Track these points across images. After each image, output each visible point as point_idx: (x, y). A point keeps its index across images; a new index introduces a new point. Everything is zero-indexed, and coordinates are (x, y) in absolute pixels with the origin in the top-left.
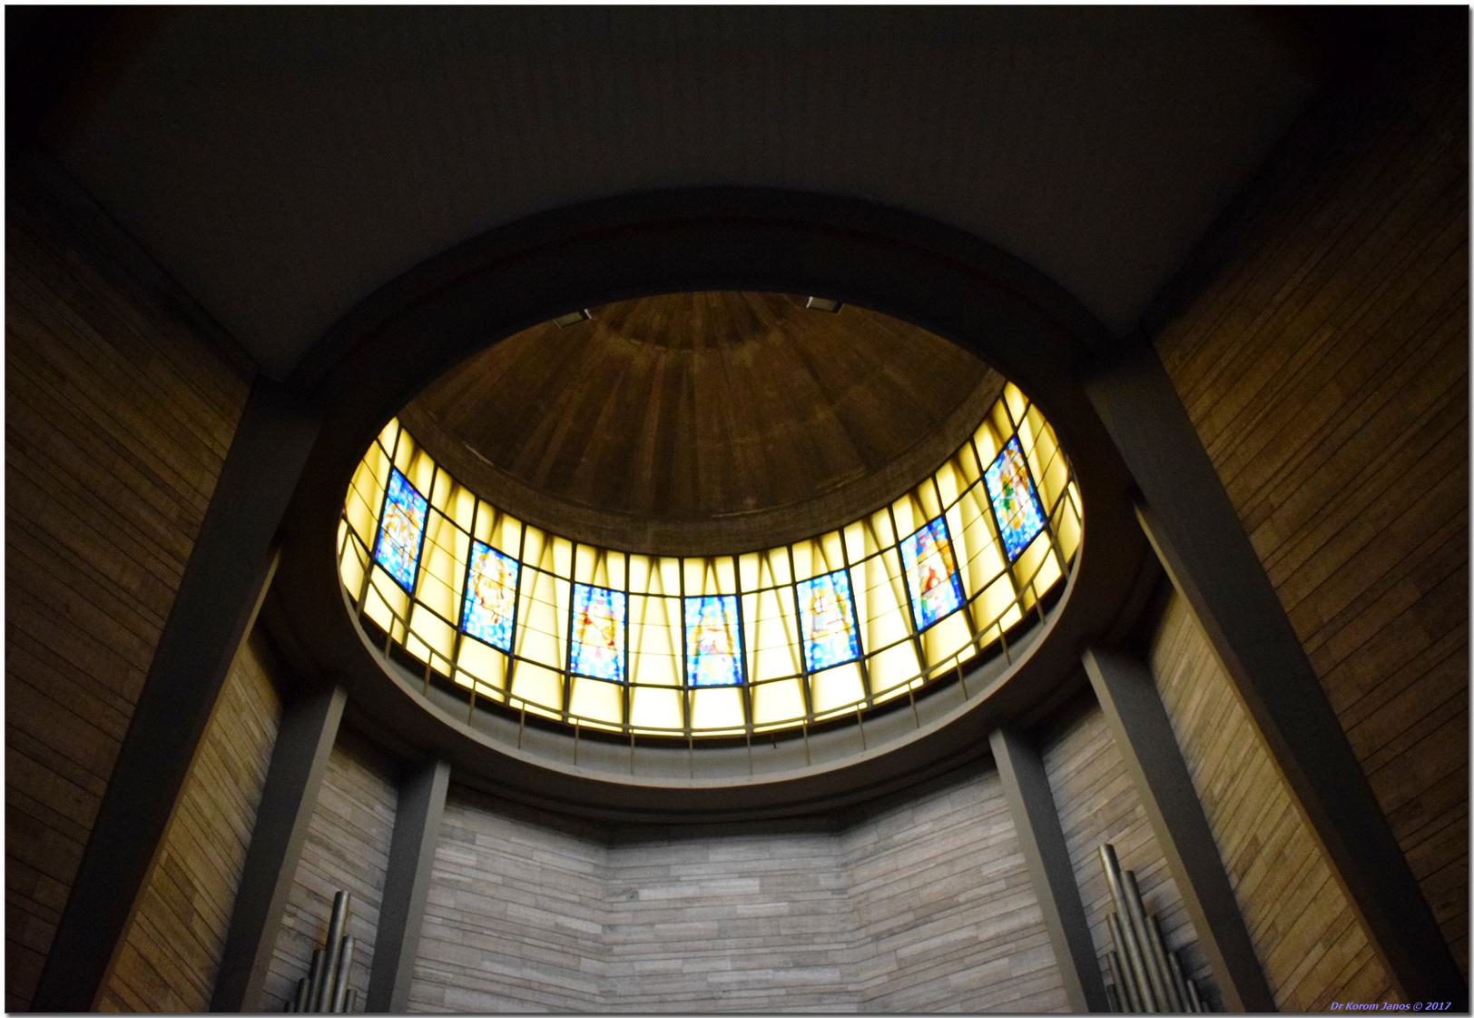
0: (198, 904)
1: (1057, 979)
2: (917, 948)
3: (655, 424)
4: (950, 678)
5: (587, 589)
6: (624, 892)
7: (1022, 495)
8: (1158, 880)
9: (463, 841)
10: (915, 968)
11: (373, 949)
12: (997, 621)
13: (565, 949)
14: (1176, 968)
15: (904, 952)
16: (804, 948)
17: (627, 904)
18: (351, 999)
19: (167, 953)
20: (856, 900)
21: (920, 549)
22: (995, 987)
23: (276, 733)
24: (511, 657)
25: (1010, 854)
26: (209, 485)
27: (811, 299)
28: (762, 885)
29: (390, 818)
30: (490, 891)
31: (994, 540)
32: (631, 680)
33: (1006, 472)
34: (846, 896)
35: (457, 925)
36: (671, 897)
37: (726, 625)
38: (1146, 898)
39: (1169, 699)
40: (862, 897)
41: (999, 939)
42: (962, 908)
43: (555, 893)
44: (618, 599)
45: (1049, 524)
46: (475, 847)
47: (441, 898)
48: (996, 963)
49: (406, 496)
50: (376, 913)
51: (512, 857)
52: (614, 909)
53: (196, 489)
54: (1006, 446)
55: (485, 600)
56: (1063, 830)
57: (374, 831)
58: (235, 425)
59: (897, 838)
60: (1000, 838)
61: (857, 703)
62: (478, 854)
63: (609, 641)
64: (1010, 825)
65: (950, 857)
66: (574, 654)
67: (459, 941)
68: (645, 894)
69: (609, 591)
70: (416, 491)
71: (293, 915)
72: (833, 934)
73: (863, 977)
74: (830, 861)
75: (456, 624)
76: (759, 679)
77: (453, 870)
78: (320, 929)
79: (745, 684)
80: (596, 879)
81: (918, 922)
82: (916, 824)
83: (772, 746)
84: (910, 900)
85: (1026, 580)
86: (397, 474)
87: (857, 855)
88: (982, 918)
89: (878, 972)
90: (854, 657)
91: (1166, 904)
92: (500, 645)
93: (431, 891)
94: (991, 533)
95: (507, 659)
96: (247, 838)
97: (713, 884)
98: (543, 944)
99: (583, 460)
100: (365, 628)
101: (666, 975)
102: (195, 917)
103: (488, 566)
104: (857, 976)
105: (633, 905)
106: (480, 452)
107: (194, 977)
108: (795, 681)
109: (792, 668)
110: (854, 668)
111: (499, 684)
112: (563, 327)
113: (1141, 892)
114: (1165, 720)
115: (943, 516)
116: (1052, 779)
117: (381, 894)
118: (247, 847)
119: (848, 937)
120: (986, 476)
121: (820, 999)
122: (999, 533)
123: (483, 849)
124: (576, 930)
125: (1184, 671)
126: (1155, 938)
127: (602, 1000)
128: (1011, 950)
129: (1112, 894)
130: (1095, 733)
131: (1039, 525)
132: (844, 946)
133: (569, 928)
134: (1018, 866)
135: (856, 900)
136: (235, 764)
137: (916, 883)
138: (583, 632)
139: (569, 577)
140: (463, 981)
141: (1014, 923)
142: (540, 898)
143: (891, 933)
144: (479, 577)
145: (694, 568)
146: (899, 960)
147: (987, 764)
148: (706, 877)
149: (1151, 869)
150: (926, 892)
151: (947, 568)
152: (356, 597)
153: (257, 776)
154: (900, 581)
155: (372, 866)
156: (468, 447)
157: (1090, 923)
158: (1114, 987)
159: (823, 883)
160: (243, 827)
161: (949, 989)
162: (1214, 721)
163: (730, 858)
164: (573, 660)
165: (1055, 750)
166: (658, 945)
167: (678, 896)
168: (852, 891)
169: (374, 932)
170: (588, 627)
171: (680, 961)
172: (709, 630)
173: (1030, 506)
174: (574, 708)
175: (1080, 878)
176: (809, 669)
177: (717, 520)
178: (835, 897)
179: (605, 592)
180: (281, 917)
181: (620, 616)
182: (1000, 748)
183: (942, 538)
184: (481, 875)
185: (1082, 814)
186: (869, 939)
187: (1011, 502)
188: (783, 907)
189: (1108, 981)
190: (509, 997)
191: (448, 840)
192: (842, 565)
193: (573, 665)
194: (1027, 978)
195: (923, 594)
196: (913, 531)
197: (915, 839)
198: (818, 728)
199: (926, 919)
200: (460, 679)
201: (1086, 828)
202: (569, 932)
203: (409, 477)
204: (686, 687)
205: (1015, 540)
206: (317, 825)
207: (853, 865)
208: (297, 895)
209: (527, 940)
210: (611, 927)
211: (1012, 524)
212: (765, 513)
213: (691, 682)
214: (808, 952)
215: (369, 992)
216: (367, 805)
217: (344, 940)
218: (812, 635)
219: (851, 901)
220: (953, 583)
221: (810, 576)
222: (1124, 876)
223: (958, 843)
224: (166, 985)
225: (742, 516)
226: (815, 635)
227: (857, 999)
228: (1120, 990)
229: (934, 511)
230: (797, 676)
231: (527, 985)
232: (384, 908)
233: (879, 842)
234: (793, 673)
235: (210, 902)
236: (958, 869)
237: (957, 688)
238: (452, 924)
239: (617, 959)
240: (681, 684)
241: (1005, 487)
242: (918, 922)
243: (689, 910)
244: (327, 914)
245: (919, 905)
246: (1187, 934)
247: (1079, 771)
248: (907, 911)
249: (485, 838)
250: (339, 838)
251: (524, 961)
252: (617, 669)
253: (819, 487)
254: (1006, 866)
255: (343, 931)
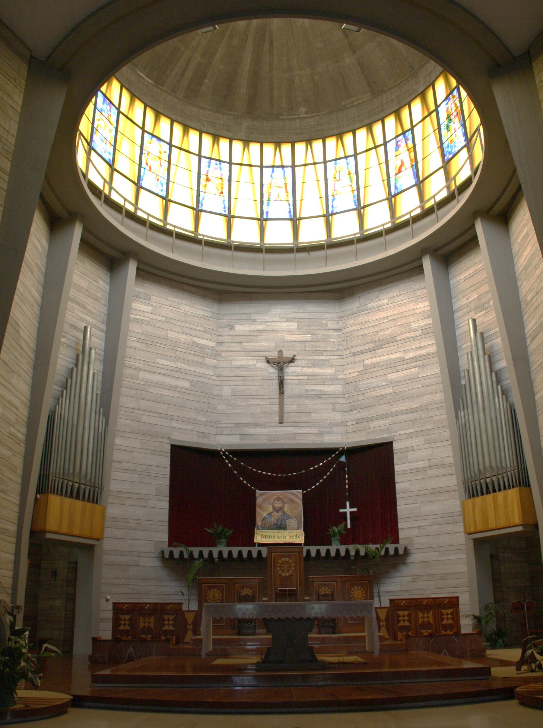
0: (22, 333)
1: (440, 379)
2: (375, 360)
3: (249, 60)
4: (405, 224)
5: (208, 160)
6: (227, 326)
7: (456, 124)
8: (494, 337)
9: (145, 299)
10: (372, 370)
11: (103, 352)
12: (434, 197)
13: (197, 354)
14: (494, 379)
15: (368, 362)
16: (318, 358)
17: (228, 332)
18: (96, 377)
19: (12, 357)
20: (346, 335)
21: (397, 146)
22: (410, 381)
23: (106, 318)
24: (167, 200)
25: (425, 318)
26: (14, 128)
27: (344, 25)
28: (298, 326)
29: (107, 287)
30: (160, 325)
31: (438, 148)
32: (232, 214)
33: (450, 109)
34: (341, 333)
35: (144, 341)
36: (251, 329)
37: (286, 184)
38: (487, 346)
39: (515, 248)
40: (349, 334)
41: (415, 359)
42: (398, 343)
43: (191, 326)
44: (226, 166)
45: (469, 145)
46: (151, 303)
47: (134, 328)
48: (412, 370)
49: (106, 107)
50: (103, 335)
51: (169, 308)
52: (222, 335)
53: (8, 132)
54: (451, 93)
55: (151, 167)
56: (453, 307)
57: (99, 295)
58: (23, 91)
59: (369, 305)
60: (421, 310)
61: (355, 234)
62: (152, 306)
63: (220, 191)
64: (427, 303)
65: (396, 317)
66: (201, 198)
67: (145, 349)
68: (238, 327)
69: (220, 161)
70: (111, 103)
71: (65, 337)
72: (332, 351)
73: (345, 372)
74: (335, 315)
75: (136, 182)
76: (302, 216)
77: (140, 314)
78: (78, 344)
79: (295, 219)
80: (213, 320)
81: (375, 348)
82: (380, 299)
83: (307, 254)
84: (373, 337)
85: (453, 174)
86: (101, 93)
87: (349, 312)
88: (407, 348)
89: (354, 371)
90: (355, 207)
91: (496, 349)
92: (160, 194)
93: (130, 325)
94: (438, 145)
95: (164, 201)
96: (39, 299)
97: (273, 324)
98: (186, 351)
99: (206, 81)
100: (91, 190)
101: (247, 367)
102: (22, 340)
103: (151, 145)
104: (343, 372)
105: (232, 333)
106: (146, 75)
107: (24, 367)
108: (322, 218)
109: (322, 211)
110: (355, 213)
111: (161, 217)
112: (202, 33)
113: (485, 342)
114: (512, 258)
115: (412, 129)
116: (452, 282)
117: (105, 326)
118: (40, 304)
119: (340, 353)
120: (439, 109)
121: (324, 382)
122: (442, 144)
123: (154, 304)
124: (203, 345)
125: (524, 236)
126: (487, 365)
127: (216, 378)
128: (419, 364)
129: (471, 343)
130: (476, 260)
131: (464, 143)
132: (338, 357)
133: (199, 344)
134: (429, 325)
135: (346, 335)
136: (31, 263)
137: (377, 329)
138: (205, 186)
139: (197, 153)
140: (147, 368)
141: (423, 352)
142: (184, 328)
143: (362, 352)
144: (148, 154)
145: (269, 148)
146: (364, 366)
147: (420, 270)
148: (270, 321)
149: (491, 332)
150: (381, 334)
151: (411, 161)
152: (84, 171)
153: (38, 264)
154: (384, 166)
155: (100, 312)
156: (139, 72)
157: (459, 354)
158: (465, 385)
159: (330, 326)
160: (37, 295)
161: (387, 381)
162: (534, 264)
163: (282, 311)
164: (200, 202)
165: (455, 267)
166: (244, 353)
167: (255, 329)
168: (345, 331)
169: (103, 344)
170: (208, 183)
171: (255, 361)
172: (276, 187)
173: (460, 132)
174: (201, 231)
175: (458, 332)
176: (330, 213)
177: (283, 120)
178: (335, 333)
179: (218, 162)
180: (60, 339)
181: (226, 177)
182: (427, 263)
183: (410, 143)
184: (154, 317)
185: (464, 301)
186: (351, 355)
187: (450, 127)
188: (308, 337)
189: (463, 382)
190: (170, 376)
191: (137, 299)
192: (352, 153)
193: (200, 205)
194: (425, 378)
195: (396, 174)
196: (394, 136)
197: (378, 307)
198: (333, 245)
199: (380, 347)
200: (140, 214)
201: (465, 309)
202: (199, 345)
203: (108, 95)
204: (262, 219)
205: (449, 150)
206: (73, 292)
207: (346, 318)
208: (66, 327)
209: (178, 349)
210: (221, 343)
211: (449, 141)
212: (311, 117)
213: (265, 217)
214: (320, 360)
215: (103, 372)
216: (95, 281)
217: (90, 349)
218: (333, 193)
219: (343, 335)
220: (413, 170)
221: (334, 158)
222: (478, 334)
223: (401, 311)
224: (13, 372)
225: (298, 118)
226: (335, 193)
227: (342, 383)
228: (467, 387)
229: (407, 126)
230: (323, 216)
231: (179, 370)
232: (107, 332)
233: (360, 306)
234: (321, 214)
235: (27, 332)
236: (399, 323)
237: (408, 229)
238: (141, 341)
239: (223, 359)
240: (259, 217)
241: (448, 117)
242: (375, 348)
243: (261, 336)
244: (81, 336)
245: (377, 340)
246: (502, 364)
247: (466, 279)
248: (371, 342)
249: (155, 297)
250: (83, 299)
251: (177, 359)
252: (225, 208)
253: (343, 103)
254: (423, 323)
255: (90, 345)
